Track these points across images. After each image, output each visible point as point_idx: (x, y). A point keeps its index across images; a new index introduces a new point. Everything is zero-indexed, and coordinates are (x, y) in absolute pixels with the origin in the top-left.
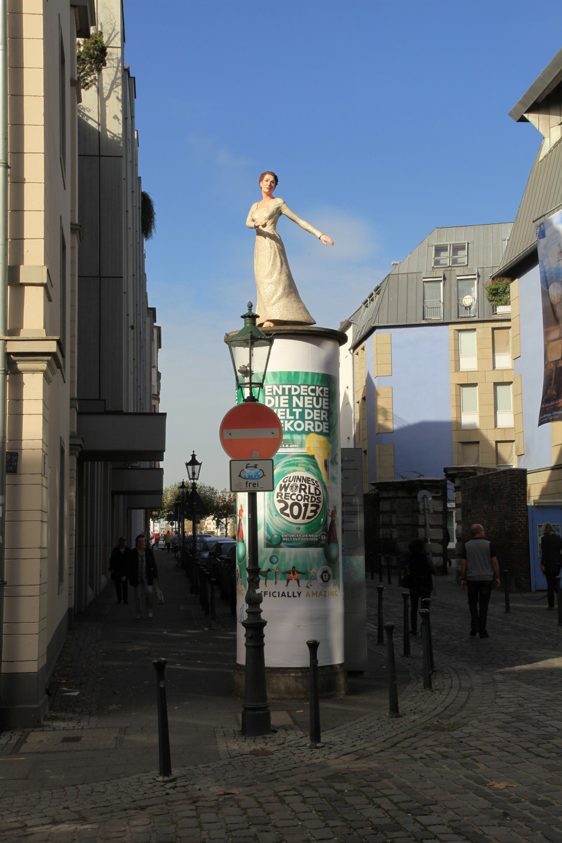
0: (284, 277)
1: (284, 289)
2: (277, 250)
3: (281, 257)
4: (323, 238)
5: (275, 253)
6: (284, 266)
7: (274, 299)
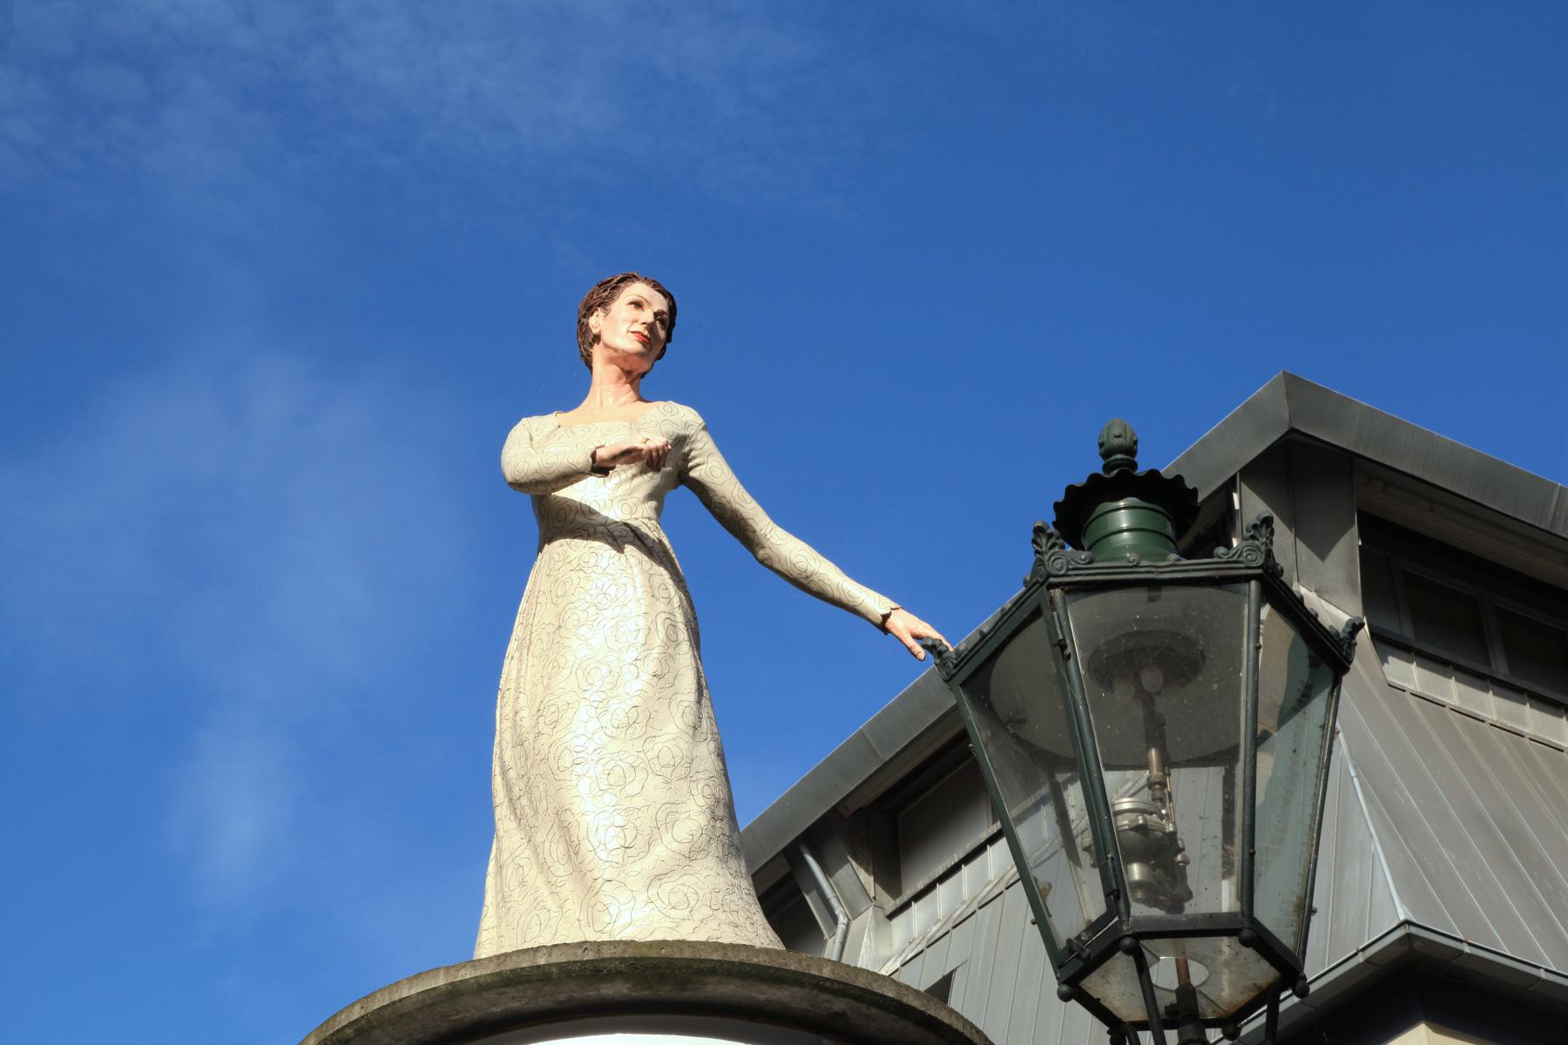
4: (905, 624)
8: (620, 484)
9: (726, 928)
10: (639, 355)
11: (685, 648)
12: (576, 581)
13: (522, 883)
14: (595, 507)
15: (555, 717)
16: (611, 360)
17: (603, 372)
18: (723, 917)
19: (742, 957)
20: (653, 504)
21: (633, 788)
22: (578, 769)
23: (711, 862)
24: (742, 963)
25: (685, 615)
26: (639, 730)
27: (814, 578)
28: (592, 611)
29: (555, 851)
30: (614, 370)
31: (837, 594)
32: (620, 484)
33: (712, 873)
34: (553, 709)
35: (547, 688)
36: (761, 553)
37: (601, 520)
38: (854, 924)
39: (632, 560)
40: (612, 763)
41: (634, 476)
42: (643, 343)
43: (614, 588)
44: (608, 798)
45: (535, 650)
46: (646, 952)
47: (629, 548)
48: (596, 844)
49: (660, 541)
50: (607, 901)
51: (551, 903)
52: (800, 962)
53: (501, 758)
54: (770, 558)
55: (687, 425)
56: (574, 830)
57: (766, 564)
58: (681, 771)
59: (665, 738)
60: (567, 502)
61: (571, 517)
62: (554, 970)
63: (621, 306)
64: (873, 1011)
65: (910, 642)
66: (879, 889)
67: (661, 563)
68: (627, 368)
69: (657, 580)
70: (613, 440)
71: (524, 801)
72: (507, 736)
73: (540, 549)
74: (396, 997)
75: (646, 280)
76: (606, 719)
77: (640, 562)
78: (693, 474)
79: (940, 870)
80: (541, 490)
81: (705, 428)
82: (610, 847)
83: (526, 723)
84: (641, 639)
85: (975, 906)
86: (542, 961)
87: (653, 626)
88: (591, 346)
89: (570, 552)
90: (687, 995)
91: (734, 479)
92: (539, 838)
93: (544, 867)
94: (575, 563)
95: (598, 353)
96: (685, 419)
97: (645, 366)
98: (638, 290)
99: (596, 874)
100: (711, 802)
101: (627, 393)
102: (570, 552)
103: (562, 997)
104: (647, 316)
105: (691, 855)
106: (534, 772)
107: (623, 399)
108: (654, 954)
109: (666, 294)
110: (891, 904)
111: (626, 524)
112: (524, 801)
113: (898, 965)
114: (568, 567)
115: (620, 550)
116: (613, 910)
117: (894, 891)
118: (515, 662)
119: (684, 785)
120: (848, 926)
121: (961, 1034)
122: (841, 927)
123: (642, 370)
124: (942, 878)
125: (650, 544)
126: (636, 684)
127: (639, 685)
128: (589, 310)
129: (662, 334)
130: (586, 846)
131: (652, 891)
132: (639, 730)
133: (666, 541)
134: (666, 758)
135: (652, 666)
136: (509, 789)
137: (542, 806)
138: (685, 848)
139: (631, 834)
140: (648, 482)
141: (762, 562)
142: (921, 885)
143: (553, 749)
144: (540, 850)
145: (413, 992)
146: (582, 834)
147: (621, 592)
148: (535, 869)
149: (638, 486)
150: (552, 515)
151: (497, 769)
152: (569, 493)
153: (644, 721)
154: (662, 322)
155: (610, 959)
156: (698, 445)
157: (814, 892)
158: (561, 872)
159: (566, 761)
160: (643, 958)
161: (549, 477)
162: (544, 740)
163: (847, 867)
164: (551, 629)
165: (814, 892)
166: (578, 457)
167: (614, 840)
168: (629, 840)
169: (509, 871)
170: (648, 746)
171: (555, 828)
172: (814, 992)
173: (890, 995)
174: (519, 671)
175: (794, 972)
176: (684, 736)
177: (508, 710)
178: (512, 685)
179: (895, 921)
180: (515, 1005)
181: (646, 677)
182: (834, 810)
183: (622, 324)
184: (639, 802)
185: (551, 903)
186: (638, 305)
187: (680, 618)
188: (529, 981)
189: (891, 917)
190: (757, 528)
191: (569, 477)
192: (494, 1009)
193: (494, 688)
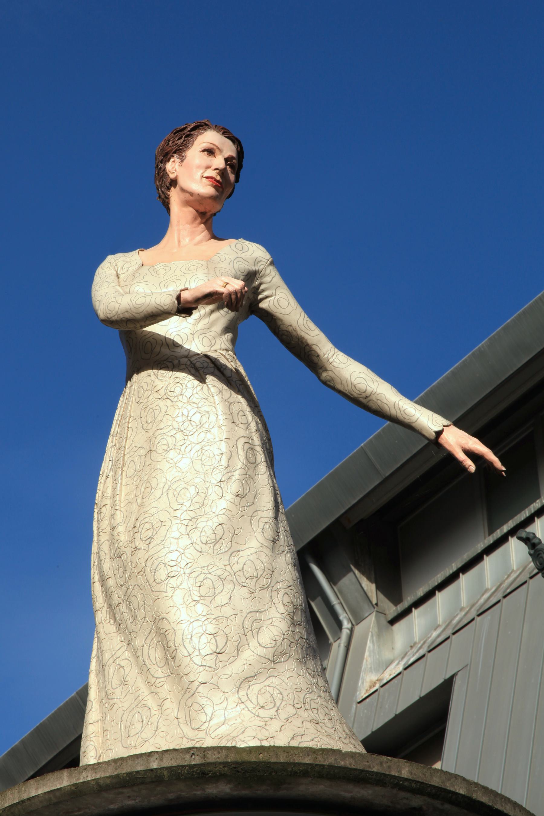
9: (308, 725)
10: (213, 198)
11: (263, 468)
12: (164, 409)
13: (124, 682)
14: (178, 340)
15: (149, 533)
16: (187, 203)
17: (179, 212)
18: (305, 714)
19: (330, 760)
20: (229, 336)
21: (221, 599)
22: (172, 581)
23: (292, 664)
24: (330, 766)
25: (261, 438)
26: (225, 545)
27: (373, 397)
28: (179, 436)
29: (154, 655)
30: (190, 212)
31: (393, 412)
32: (200, 319)
33: (294, 674)
34: (147, 526)
35: (141, 506)
36: (324, 375)
38: (358, 629)
39: (213, 390)
40: (202, 577)
41: (212, 312)
42: (215, 187)
43: (198, 416)
44: (200, 608)
45: (129, 470)
46: (246, 757)
47: (210, 379)
48: (191, 650)
49: (237, 371)
50: (202, 701)
51: (151, 702)
52: (381, 764)
53: (100, 567)
54: (332, 380)
55: (257, 261)
56: (170, 637)
58: (263, 582)
59: (247, 552)
60: (155, 337)
61: (157, 349)
62: (165, 773)
63: (194, 153)
64: (447, 806)
65: (461, 456)
66: (381, 596)
67: (238, 392)
68: (202, 209)
69: (236, 408)
70: (196, 284)
71: (123, 608)
72: (105, 547)
73: (129, 378)
74: (25, 796)
76: (195, 536)
77: (221, 392)
78: (263, 305)
79: (439, 578)
80: (131, 326)
81: (272, 263)
82: (204, 653)
83: (124, 538)
84: (224, 462)
85: (473, 613)
86: (154, 765)
87: (234, 450)
88: (169, 189)
89: (157, 382)
90: (282, 793)
91: (299, 309)
92: (138, 642)
93: (144, 670)
94: (162, 392)
95: (174, 196)
96: (255, 255)
97: (218, 207)
98: (210, 137)
99: (192, 677)
100: (290, 609)
101: (201, 232)
102: (157, 382)
103: (171, 796)
104: (219, 162)
105: (275, 659)
106: (132, 582)
107: (199, 238)
108: (253, 758)
109: (235, 140)
110: (392, 610)
111: (206, 356)
112: (123, 608)
113: (400, 668)
114: (156, 396)
115: (202, 380)
116: (209, 710)
117: (396, 599)
118: (110, 481)
119: (266, 594)
120: (352, 630)
122: (345, 632)
123: (213, 211)
124: (441, 586)
125: (228, 374)
126: (221, 504)
127: (223, 504)
128: (166, 157)
129: (232, 177)
130: (182, 652)
131: (242, 693)
132: (225, 545)
133: (241, 370)
134: (250, 571)
135: (234, 487)
136: (108, 595)
137: (141, 614)
138: (269, 653)
139: (221, 641)
140: (223, 317)
141: (325, 383)
142: (421, 592)
143: (149, 563)
144: (139, 654)
145: (40, 792)
146: (178, 641)
147: (204, 419)
148: (135, 671)
150: (139, 347)
151: (95, 576)
152: (159, 329)
153: (228, 537)
154: (232, 166)
155: (215, 764)
156: (267, 279)
157: (319, 599)
158: (159, 674)
159: (162, 574)
160: (243, 763)
161: (138, 316)
162: (140, 554)
163: (350, 575)
164: (142, 452)
165: (319, 599)
166: (164, 298)
167: (206, 645)
168: (220, 647)
169: (111, 670)
170: (234, 560)
171: (153, 634)
172: (395, 791)
173: (462, 792)
174: (114, 489)
175: (377, 773)
177: (105, 524)
178: (108, 502)
179: (397, 626)
180: (130, 803)
181: (229, 496)
182: (337, 521)
183: (196, 169)
184: (227, 611)
185: (151, 702)
186: (210, 152)
187: (257, 441)
188: (142, 783)
189: (393, 622)
190: (321, 354)
191: (157, 316)
192: (112, 807)
193: (92, 503)
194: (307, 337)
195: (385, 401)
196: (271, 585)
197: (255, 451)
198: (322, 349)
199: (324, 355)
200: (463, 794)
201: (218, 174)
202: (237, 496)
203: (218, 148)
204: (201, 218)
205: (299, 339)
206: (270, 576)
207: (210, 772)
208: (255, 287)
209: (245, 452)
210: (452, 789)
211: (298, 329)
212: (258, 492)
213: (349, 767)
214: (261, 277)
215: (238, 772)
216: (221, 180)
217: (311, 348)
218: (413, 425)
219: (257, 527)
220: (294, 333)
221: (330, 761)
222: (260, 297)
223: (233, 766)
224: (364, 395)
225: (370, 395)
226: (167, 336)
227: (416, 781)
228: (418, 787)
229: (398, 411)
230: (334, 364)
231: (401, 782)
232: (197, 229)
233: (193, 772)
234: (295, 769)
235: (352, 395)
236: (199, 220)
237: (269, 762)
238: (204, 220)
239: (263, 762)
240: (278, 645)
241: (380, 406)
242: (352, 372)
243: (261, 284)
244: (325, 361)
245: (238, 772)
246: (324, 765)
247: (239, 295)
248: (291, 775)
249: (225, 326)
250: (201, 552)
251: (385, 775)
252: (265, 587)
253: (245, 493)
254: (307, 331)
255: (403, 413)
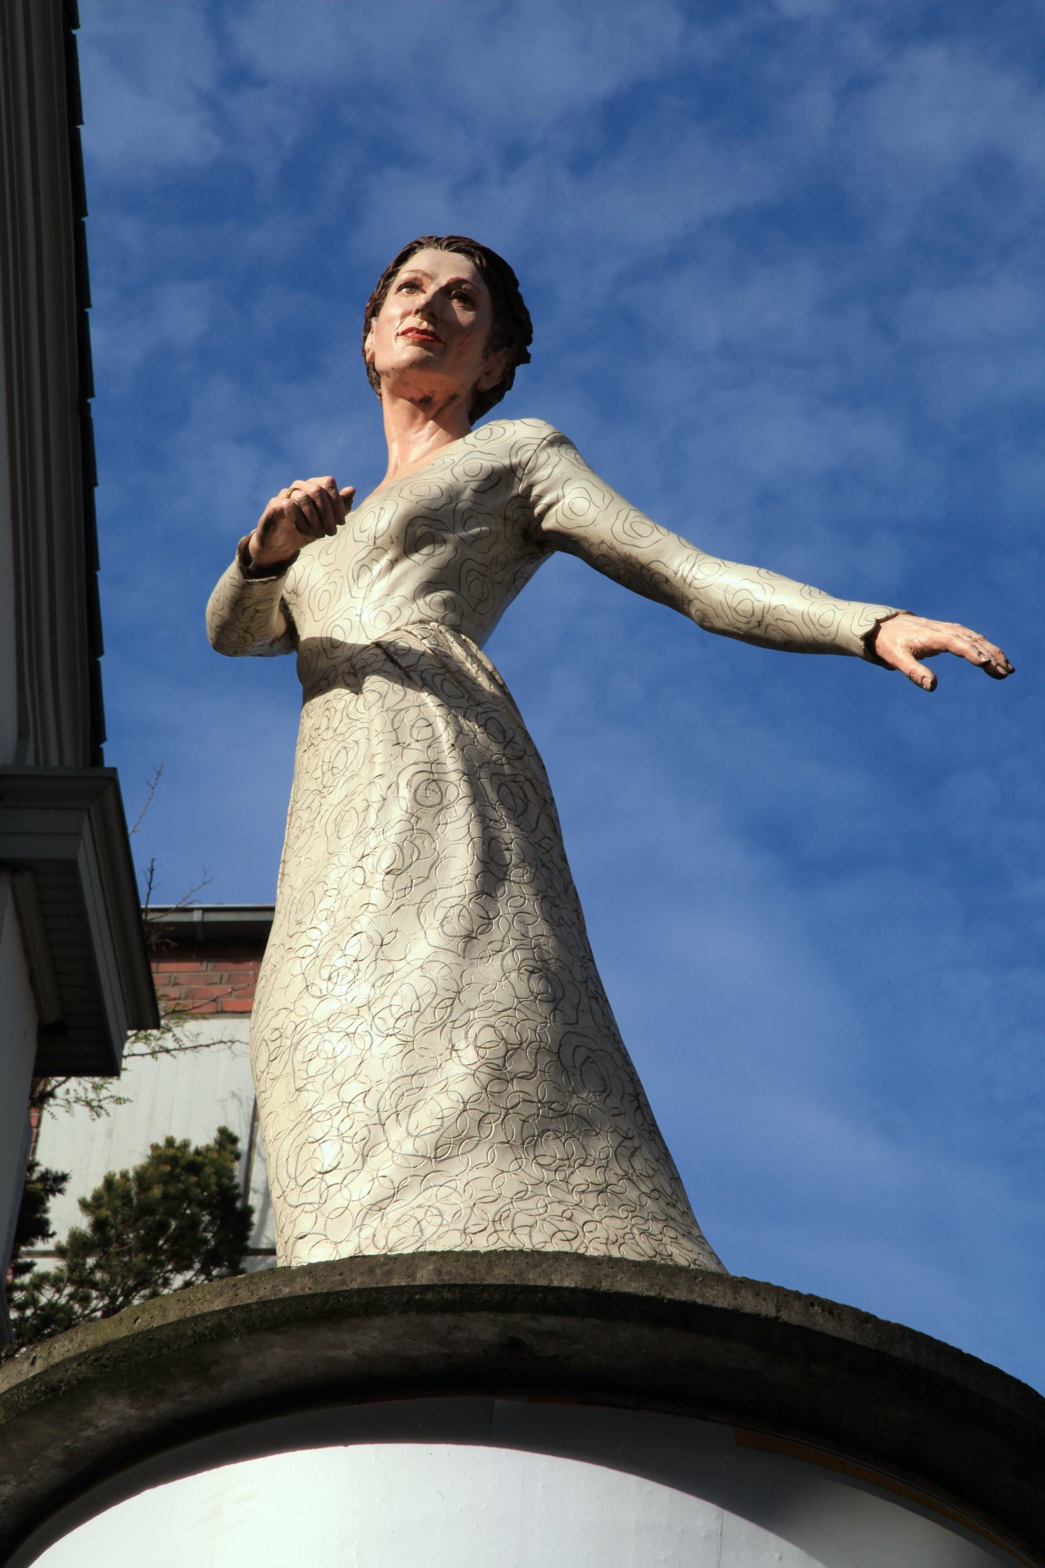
0: (501, 978)
1: (498, 1072)
2: (452, 764)
3: (484, 819)
4: (903, 636)
5: (432, 777)
6: (519, 893)
7: (386, 1163)
8: (372, 584)
24: (263, 1304)
27: (769, 619)
31: (807, 632)
37: (347, 653)
41: (393, 563)
42: (421, 343)
57: (708, 626)
68: (418, 396)
75: (436, 242)
78: (548, 524)
105: (440, 1153)
121: (774, 1322)
149: (404, 574)
156: (542, 474)
175: (359, 1291)
176: (447, 958)
190: (669, 573)
194: (635, 552)
195: (788, 617)
196: (452, 1019)
197: (441, 784)
198: (669, 564)
199: (676, 574)
200: (573, 1285)
201: (423, 318)
202: (388, 873)
203: (426, 275)
204: (424, 411)
205: (624, 561)
206: (448, 1002)
207: (61, 1382)
208: (518, 496)
209: (412, 790)
210: (542, 1282)
211: (616, 543)
212: (442, 856)
213: (301, 1293)
214: (529, 472)
215: (106, 1367)
216: (431, 328)
217: (650, 570)
218: (838, 641)
219: (432, 920)
220: (614, 554)
221: (262, 1293)
222: (538, 510)
223: (92, 1357)
224: (754, 621)
225: (763, 617)
226: (324, 635)
227: (450, 1286)
228: (458, 1296)
229: (812, 626)
230: (696, 583)
231: (418, 1296)
232: (421, 433)
233: (36, 1392)
234: (199, 1328)
235: (739, 629)
236: (421, 415)
237: (148, 1330)
238: (432, 413)
239: (139, 1334)
240: (446, 1125)
241: (785, 629)
242: (729, 585)
243: (531, 486)
244: (680, 584)
245: (106, 1367)
246: (248, 1305)
247: (318, 503)
248: (195, 1342)
249: (424, 580)
250: (319, 997)
251: (378, 1290)
252: (435, 1025)
253: (407, 863)
254: (636, 542)
255: (818, 627)
